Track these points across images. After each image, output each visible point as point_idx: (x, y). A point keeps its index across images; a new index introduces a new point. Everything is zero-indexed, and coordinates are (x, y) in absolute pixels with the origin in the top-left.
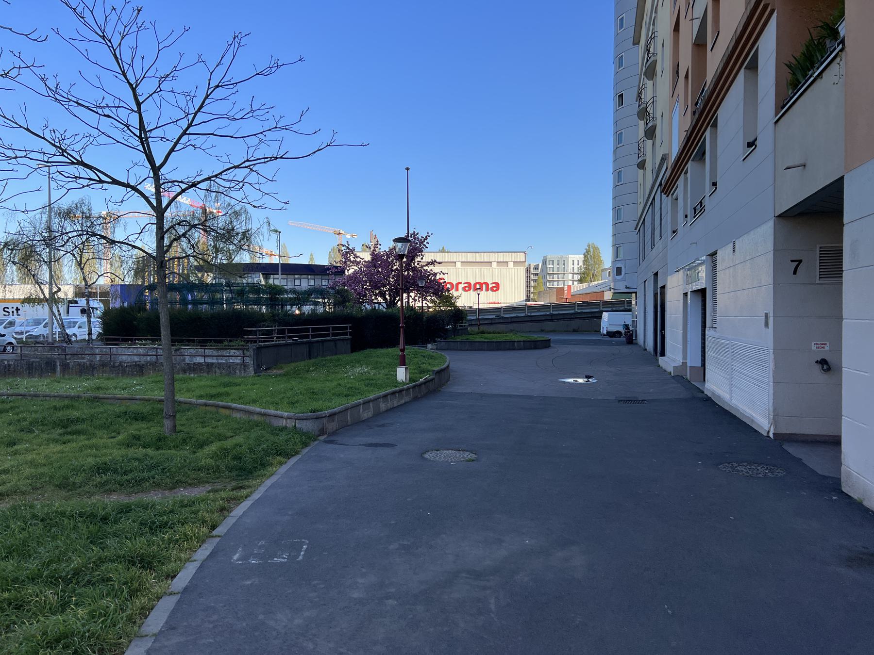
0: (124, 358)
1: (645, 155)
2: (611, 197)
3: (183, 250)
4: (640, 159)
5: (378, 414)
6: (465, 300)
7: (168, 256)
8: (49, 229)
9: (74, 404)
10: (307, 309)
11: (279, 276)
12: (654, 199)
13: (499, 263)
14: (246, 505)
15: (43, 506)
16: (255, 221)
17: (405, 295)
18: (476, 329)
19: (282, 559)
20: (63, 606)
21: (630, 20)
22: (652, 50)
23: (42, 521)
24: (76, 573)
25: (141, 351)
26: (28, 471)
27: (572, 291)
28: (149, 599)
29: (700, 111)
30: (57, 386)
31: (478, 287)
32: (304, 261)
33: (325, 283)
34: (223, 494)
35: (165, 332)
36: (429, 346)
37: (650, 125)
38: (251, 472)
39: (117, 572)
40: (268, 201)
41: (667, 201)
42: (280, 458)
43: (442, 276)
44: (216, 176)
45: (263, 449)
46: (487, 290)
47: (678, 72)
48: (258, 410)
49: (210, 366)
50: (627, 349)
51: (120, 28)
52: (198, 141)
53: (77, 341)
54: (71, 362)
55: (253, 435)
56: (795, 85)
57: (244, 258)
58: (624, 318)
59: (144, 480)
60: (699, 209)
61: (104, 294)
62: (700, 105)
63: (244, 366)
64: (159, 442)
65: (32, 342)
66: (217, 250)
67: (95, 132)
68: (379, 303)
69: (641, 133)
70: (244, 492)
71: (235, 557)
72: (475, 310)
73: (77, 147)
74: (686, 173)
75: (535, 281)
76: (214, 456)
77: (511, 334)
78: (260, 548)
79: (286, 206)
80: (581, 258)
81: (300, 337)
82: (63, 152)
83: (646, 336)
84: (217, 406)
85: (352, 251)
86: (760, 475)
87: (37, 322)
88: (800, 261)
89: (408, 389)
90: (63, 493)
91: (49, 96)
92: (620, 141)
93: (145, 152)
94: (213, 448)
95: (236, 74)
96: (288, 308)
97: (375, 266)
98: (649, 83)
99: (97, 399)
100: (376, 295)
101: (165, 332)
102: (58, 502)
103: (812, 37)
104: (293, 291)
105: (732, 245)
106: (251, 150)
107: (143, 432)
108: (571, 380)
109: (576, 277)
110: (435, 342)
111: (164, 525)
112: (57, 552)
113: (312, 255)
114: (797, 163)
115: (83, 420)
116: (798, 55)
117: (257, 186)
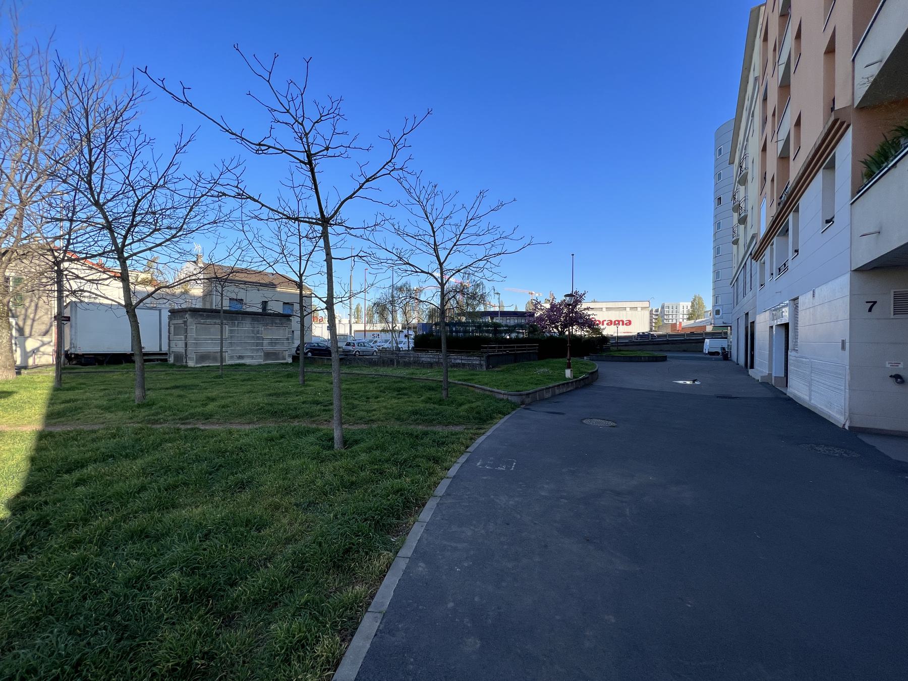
0: (423, 359)
1: (738, 235)
2: (712, 264)
3: (451, 305)
4: (735, 238)
5: (554, 396)
6: (608, 331)
7: (446, 307)
8: (393, 297)
9: (403, 380)
10: (514, 335)
11: (499, 318)
12: (745, 264)
13: (631, 308)
14: (483, 438)
15: (391, 428)
16: (488, 287)
17: (571, 328)
18: (615, 348)
19: (503, 468)
20: (400, 476)
21: (726, 149)
22: (744, 166)
23: (391, 434)
24: (405, 461)
25: (431, 356)
26: (384, 411)
27: (682, 325)
28: (438, 479)
29: (784, 202)
30: (395, 371)
31: (617, 323)
32: (512, 309)
33: (523, 321)
34: (472, 431)
35: (444, 346)
36: (585, 358)
37: (742, 215)
38: (485, 421)
39: (424, 464)
40: (496, 277)
41: (756, 265)
42: (500, 415)
43: (593, 316)
44: (469, 266)
45: (492, 410)
46: (623, 324)
47: (765, 178)
48: (489, 389)
49: (464, 365)
50: (723, 364)
51: (427, 196)
52: (461, 248)
53: (403, 351)
54: (401, 361)
55: (486, 402)
56: (870, 175)
57: (481, 308)
58: (723, 343)
59: (434, 420)
60: (783, 269)
61: (415, 328)
62: (784, 198)
63: (481, 365)
64: (440, 402)
65: (384, 351)
66: (468, 305)
67: (414, 248)
68: (555, 332)
69: (735, 221)
70: (482, 431)
71: (478, 464)
72: (615, 337)
73: (406, 256)
74: (772, 245)
75: (656, 319)
76: (467, 411)
77: (640, 352)
78: (491, 461)
79: (505, 279)
80: (690, 304)
81: (510, 351)
82: (401, 259)
83: (739, 355)
84: (468, 386)
85: (539, 303)
86: (837, 455)
87: (386, 341)
88: (875, 303)
89: (572, 382)
90: (398, 423)
92: (719, 227)
93: (436, 256)
94: (466, 407)
95: (481, 212)
96: (504, 335)
97: (552, 311)
98: (742, 188)
99: (412, 379)
100: (553, 328)
101: (444, 346)
102: (396, 426)
103: (886, 139)
104: (506, 326)
105: (812, 292)
106: (488, 251)
107: (433, 396)
108: (681, 382)
109: (685, 317)
110: (589, 355)
111: (443, 443)
112: (397, 449)
113: (516, 306)
114: (872, 231)
115: (406, 389)
116: (872, 154)
117: (490, 270)
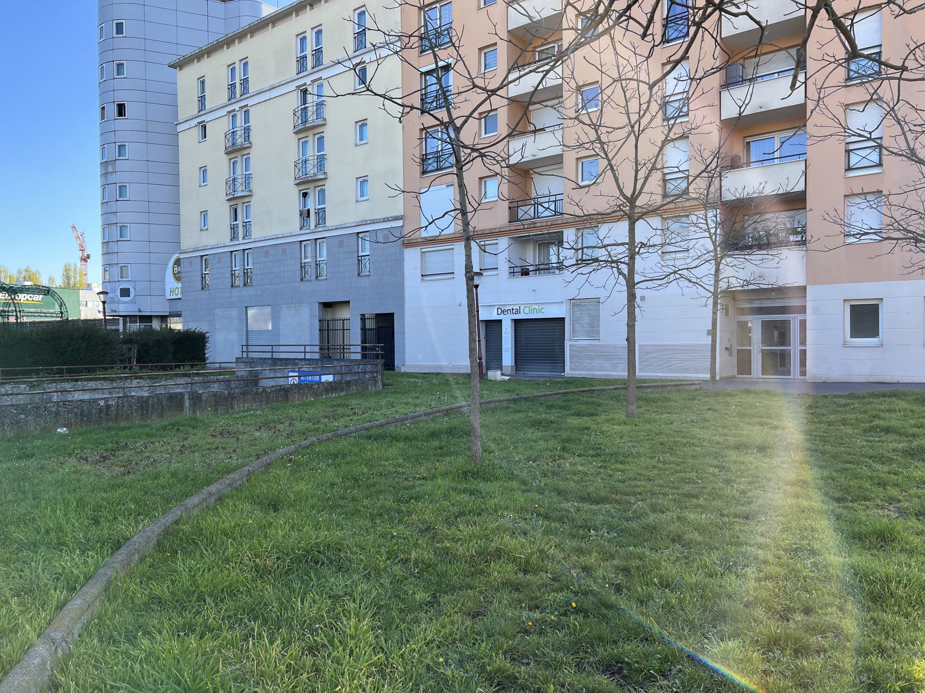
91: (800, 9)
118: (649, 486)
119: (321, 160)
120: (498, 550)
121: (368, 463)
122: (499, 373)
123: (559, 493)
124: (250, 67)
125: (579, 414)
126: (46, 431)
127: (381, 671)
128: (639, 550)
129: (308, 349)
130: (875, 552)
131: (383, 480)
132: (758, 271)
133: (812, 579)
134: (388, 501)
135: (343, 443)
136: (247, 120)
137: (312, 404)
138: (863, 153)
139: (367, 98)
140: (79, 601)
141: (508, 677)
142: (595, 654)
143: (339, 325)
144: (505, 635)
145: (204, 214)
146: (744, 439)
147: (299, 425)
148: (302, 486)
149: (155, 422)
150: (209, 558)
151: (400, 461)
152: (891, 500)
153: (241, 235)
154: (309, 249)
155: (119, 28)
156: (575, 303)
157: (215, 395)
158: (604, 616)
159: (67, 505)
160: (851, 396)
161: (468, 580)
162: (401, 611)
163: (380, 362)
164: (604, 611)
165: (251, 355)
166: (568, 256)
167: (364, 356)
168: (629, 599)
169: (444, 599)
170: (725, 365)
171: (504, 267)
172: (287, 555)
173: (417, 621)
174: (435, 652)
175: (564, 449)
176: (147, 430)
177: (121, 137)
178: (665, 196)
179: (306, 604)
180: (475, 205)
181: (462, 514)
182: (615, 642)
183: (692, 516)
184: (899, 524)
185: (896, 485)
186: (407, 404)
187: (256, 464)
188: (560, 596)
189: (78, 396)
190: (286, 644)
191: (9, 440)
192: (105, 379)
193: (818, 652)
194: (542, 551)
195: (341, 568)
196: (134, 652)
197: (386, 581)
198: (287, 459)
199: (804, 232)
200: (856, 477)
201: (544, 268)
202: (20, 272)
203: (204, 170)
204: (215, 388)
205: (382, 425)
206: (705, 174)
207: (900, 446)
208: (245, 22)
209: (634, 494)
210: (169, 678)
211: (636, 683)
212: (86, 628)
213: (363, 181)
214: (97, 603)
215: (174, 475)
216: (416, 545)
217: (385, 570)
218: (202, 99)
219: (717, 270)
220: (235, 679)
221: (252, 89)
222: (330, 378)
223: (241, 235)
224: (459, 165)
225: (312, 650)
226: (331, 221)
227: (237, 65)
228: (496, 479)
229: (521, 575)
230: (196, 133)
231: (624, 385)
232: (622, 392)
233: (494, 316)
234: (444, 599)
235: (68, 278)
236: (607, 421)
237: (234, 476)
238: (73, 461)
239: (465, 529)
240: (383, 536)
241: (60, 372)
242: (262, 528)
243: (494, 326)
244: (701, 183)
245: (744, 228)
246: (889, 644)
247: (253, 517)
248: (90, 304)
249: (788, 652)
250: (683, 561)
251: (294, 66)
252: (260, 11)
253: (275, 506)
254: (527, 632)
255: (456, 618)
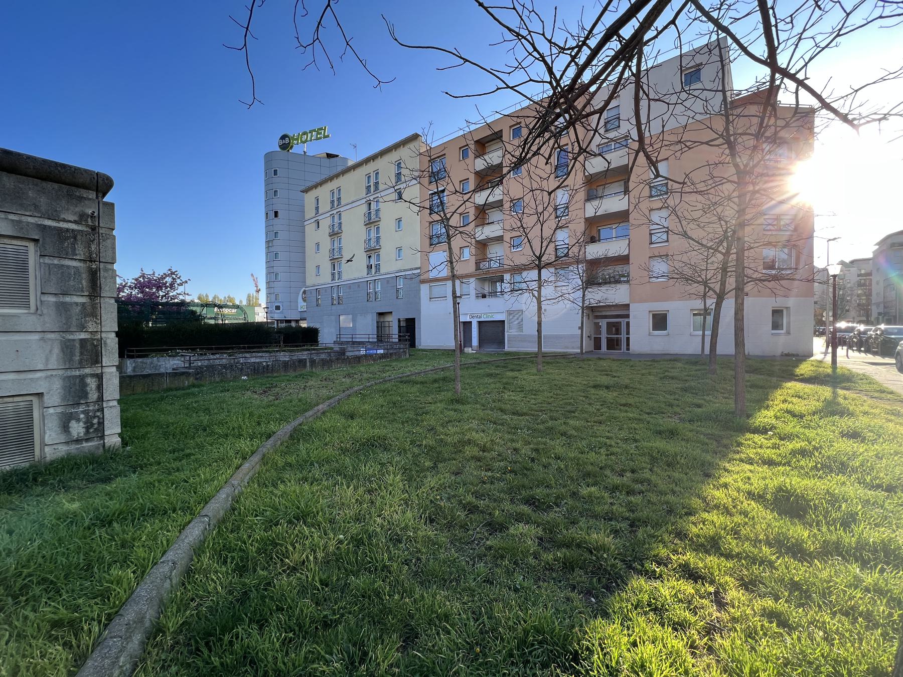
118: (549, 407)
119: (378, 239)
120: (469, 440)
121: (401, 395)
122: (470, 349)
123: (502, 410)
124: (342, 191)
125: (512, 370)
126: (236, 378)
127: (406, 503)
128: (544, 440)
129: (371, 336)
130: (668, 440)
131: (409, 404)
132: (605, 296)
133: (635, 454)
134: (411, 414)
135: (388, 385)
136: (340, 219)
137: (373, 365)
138: (659, 235)
139: (401, 204)
140: (247, 465)
141: (474, 507)
142: (521, 494)
143: (387, 324)
144: (472, 484)
145: (318, 267)
146: (599, 383)
147: (365, 375)
148: (366, 407)
149: (292, 374)
150: (317, 443)
151: (418, 394)
152: (676, 413)
153: (337, 278)
154: (371, 286)
155: (275, 172)
156: (510, 313)
157: (322, 360)
158: (525, 475)
159: (244, 415)
160: (653, 361)
161: (453, 455)
162: (417, 471)
163: (408, 343)
164: (525, 472)
165: (342, 340)
166: (506, 287)
167: (400, 340)
168: (538, 465)
169: (440, 465)
170: (588, 345)
171: (473, 293)
172: (358, 442)
173: (426, 477)
174: (435, 493)
175: (504, 388)
176: (288, 378)
177: (276, 229)
178: (556, 256)
179: (367, 468)
180: (457, 258)
181: (450, 421)
182: (531, 488)
183: (571, 422)
184: (681, 426)
185: (678, 406)
186: (422, 365)
187: (342, 395)
188: (502, 464)
189: (253, 360)
190: (356, 488)
191: (217, 383)
192: (266, 352)
193: (639, 493)
194: (492, 441)
195: (386, 449)
196: (276, 492)
197: (410, 456)
198: (357, 393)
199: (628, 276)
200: (657, 402)
201: (493, 294)
202: (225, 298)
203: (318, 244)
204: (323, 356)
205: (408, 376)
206: (577, 244)
207: (679, 386)
208: (339, 169)
209: (541, 411)
210: (293, 505)
211: (542, 509)
212: (252, 480)
213: (400, 249)
214: (258, 466)
215: (300, 400)
216: (426, 437)
217: (409, 450)
218: (317, 208)
219: (584, 295)
220: (329, 507)
221: (343, 202)
222: (381, 351)
223: (337, 278)
224: (449, 237)
225: (370, 492)
226: (382, 271)
227: (335, 191)
228: (468, 403)
229: (481, 453)
230: (314, 225)
231: (536, 355)
232: (535, 359)
233: (468, 320)
234: (440, 465)
235: (250, 301)
236: (527, 373)
237: (332, 401)
238: (249, 393)
239: (452, 429)
240: (408, 432)
241: (244, 348)
242: (345, 428)
243: (467, 325)
244: (575, 249)
245: (597, 273)
246: (677, 489)
247: (341, 422)
248: (260, 314)
249: (624, 493)
250: (567, 445)
251: (364, 191)
252: (347, 163)
253: (352, 417)
254: (484, 483)
255: (446, 475)
